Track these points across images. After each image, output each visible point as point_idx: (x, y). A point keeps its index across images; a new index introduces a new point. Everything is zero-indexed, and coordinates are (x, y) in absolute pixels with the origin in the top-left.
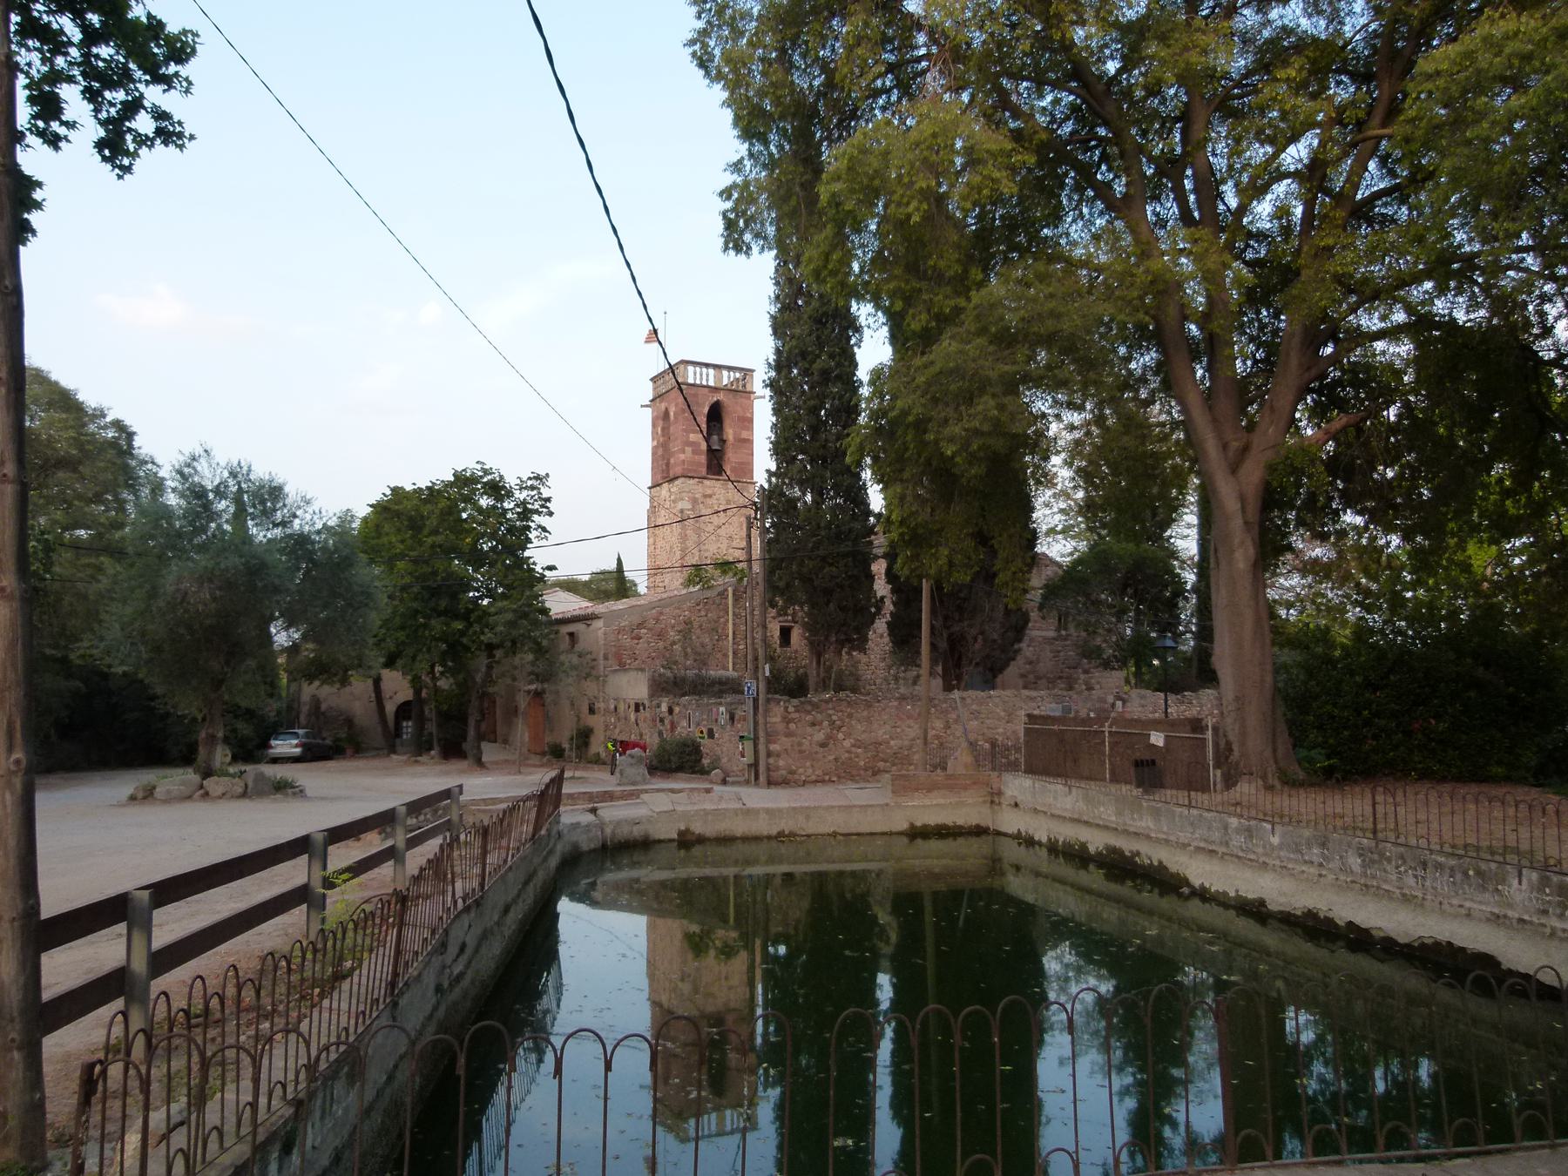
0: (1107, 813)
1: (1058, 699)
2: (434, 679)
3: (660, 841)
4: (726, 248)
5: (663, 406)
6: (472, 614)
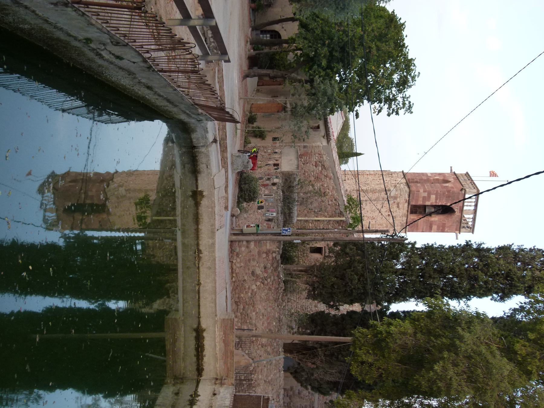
2: (294, 50)
3: (197, 180)
5: (452, 180)
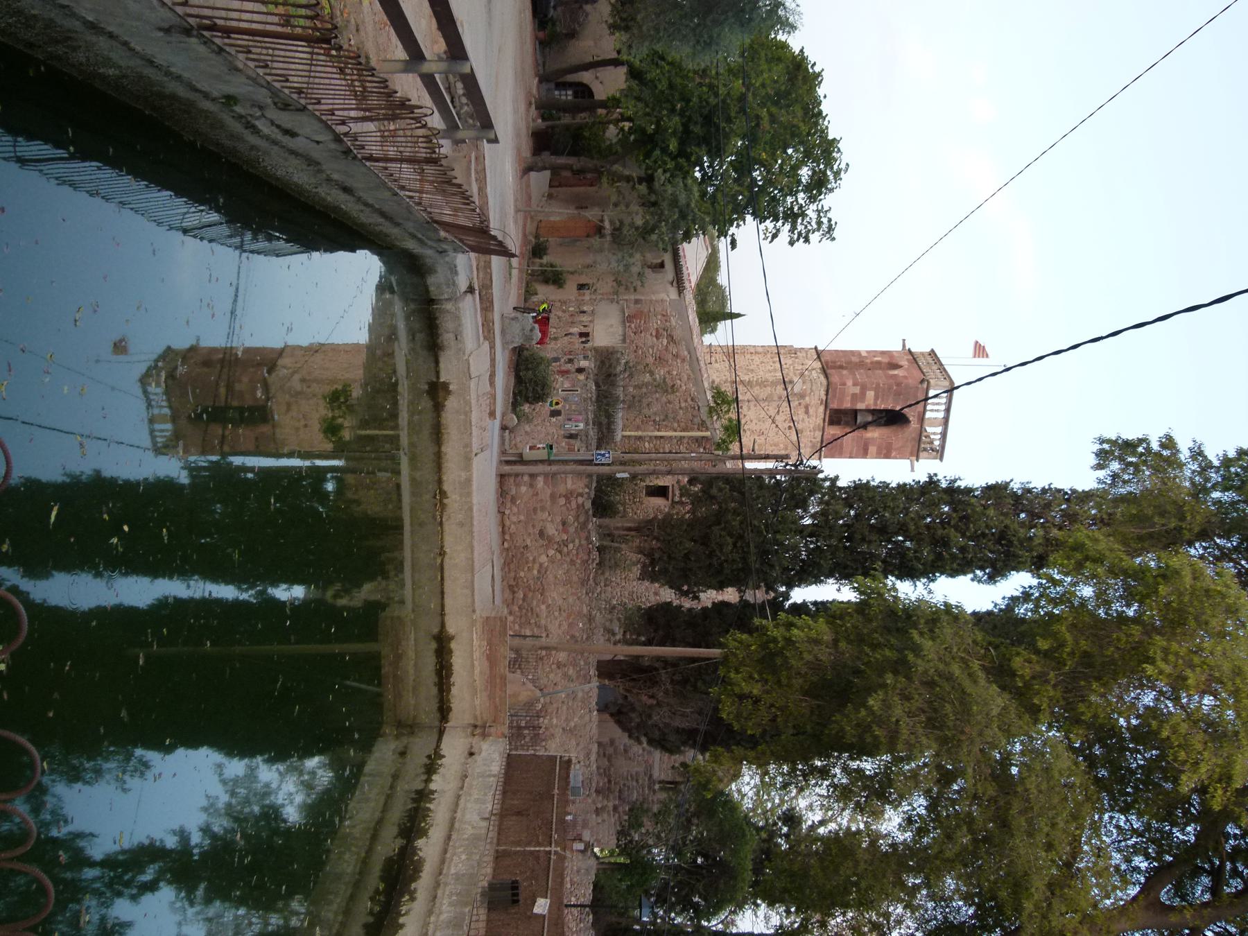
0: (458, 864)
1: (587, 782)
3: (437, 362)
4: (1102, 441)
5: (904, 363)
6: (685, 159)
